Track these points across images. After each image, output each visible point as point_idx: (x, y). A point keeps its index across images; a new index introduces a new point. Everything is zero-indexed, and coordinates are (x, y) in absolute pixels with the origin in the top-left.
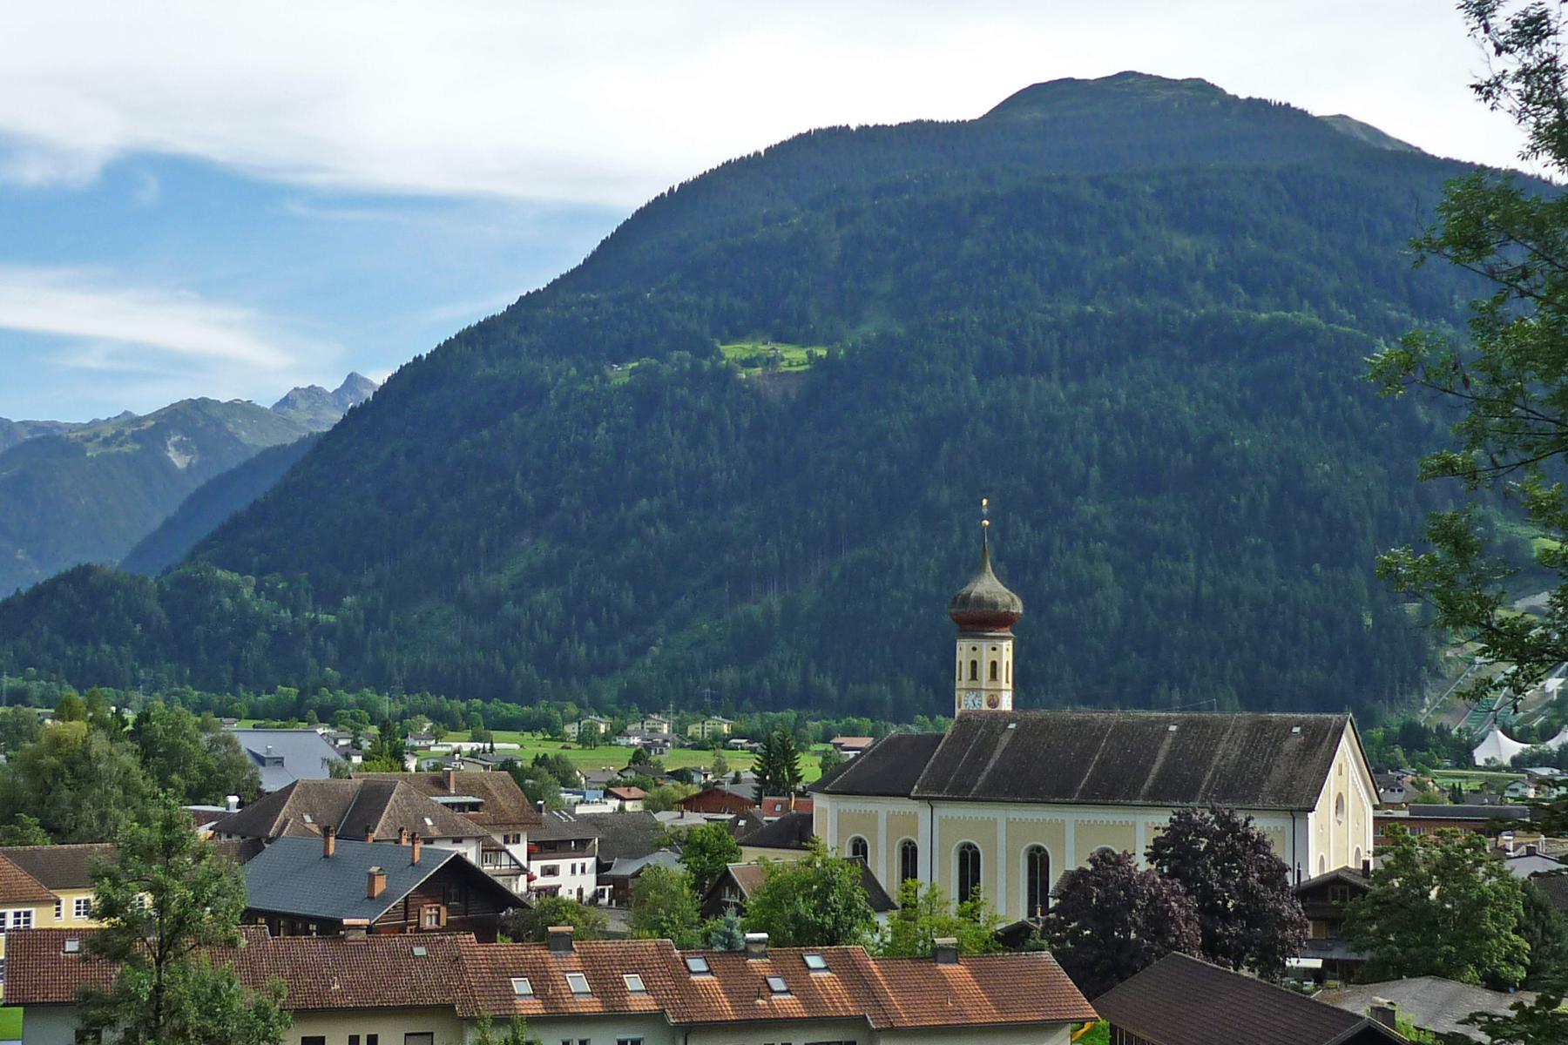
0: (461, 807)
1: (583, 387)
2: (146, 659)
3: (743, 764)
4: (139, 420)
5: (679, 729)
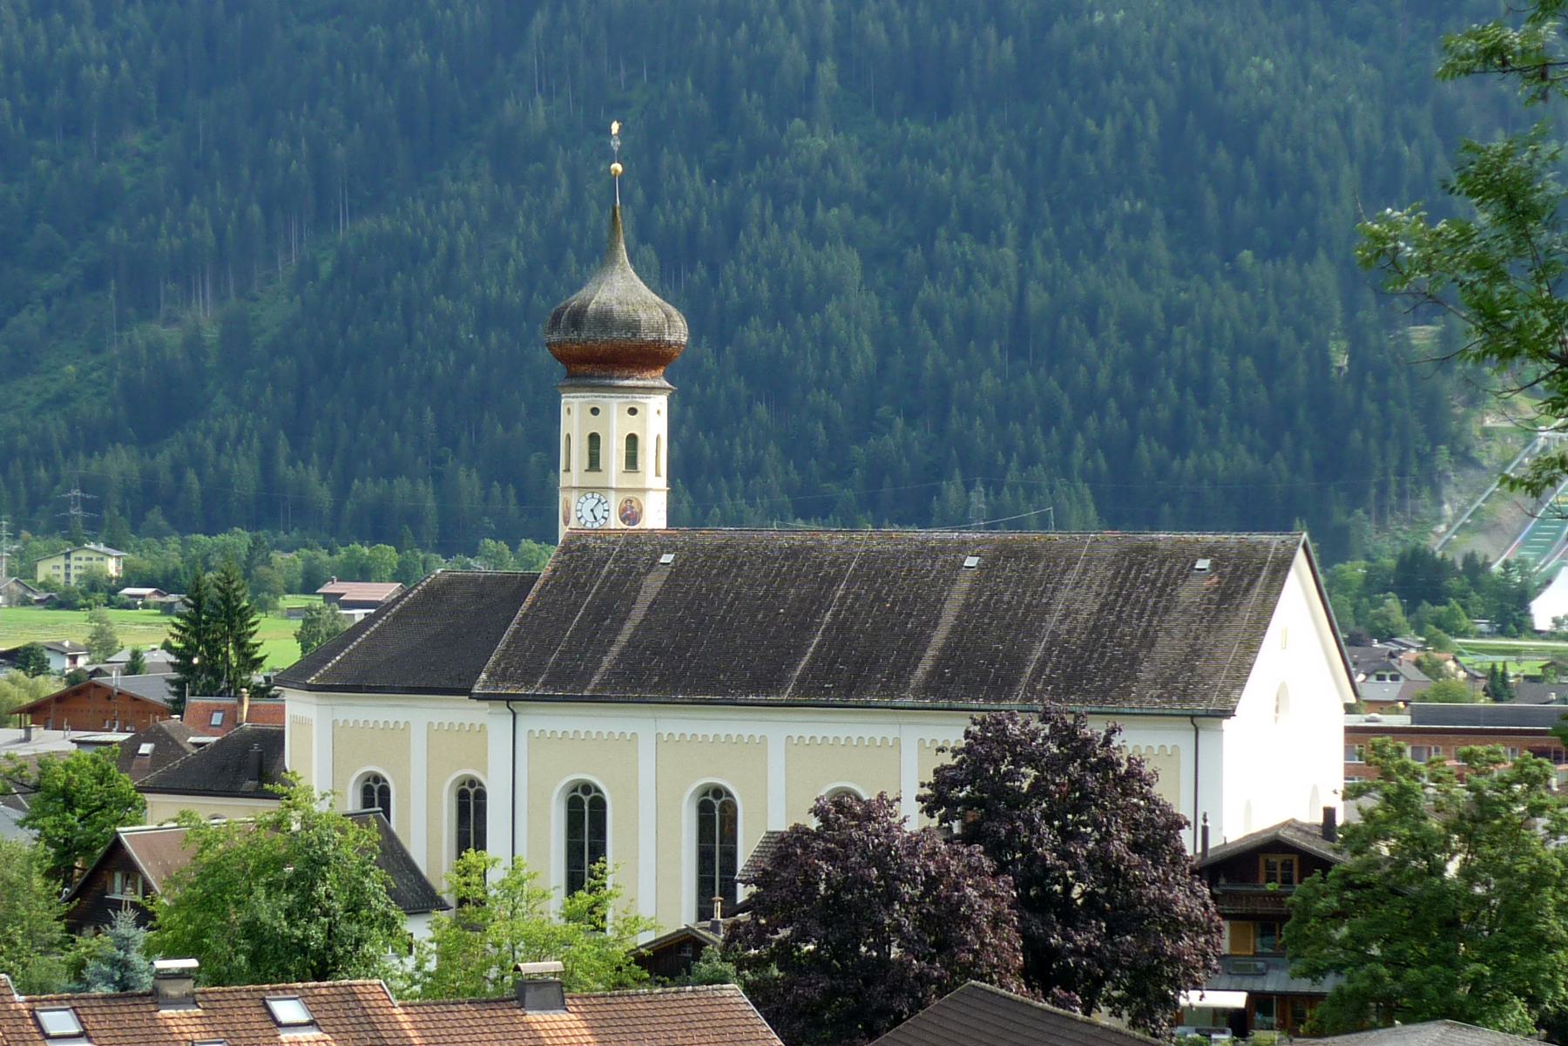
3: (147, 636)
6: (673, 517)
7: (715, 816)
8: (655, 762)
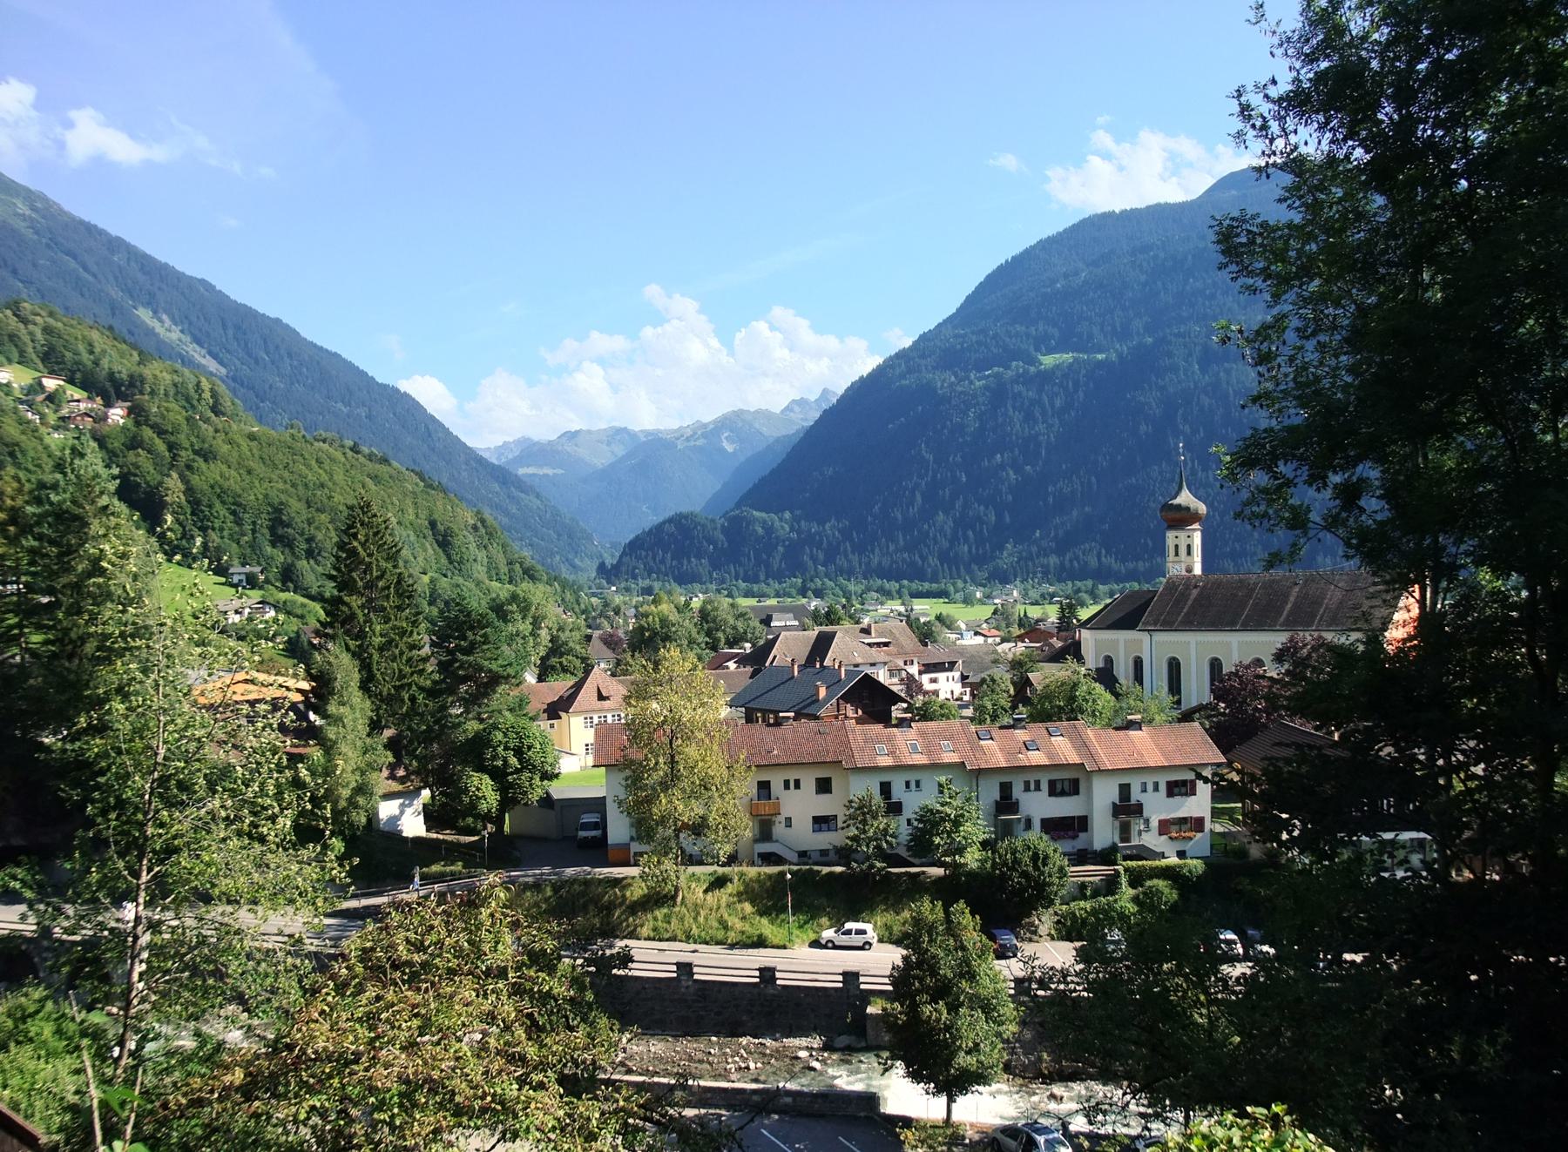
0: (878, 644)
1: (959, 389)
2: (715, 566)
3: (1052, 614)
4: (705, 426)
5: (1025, 595)
6: (1203, 570)
7: (1215, 665)
8: (1198, 649)
